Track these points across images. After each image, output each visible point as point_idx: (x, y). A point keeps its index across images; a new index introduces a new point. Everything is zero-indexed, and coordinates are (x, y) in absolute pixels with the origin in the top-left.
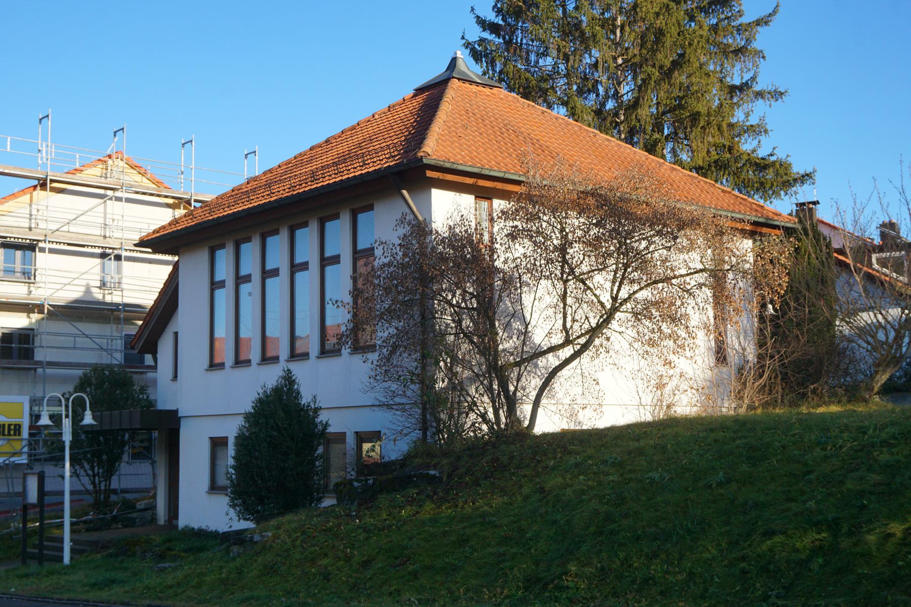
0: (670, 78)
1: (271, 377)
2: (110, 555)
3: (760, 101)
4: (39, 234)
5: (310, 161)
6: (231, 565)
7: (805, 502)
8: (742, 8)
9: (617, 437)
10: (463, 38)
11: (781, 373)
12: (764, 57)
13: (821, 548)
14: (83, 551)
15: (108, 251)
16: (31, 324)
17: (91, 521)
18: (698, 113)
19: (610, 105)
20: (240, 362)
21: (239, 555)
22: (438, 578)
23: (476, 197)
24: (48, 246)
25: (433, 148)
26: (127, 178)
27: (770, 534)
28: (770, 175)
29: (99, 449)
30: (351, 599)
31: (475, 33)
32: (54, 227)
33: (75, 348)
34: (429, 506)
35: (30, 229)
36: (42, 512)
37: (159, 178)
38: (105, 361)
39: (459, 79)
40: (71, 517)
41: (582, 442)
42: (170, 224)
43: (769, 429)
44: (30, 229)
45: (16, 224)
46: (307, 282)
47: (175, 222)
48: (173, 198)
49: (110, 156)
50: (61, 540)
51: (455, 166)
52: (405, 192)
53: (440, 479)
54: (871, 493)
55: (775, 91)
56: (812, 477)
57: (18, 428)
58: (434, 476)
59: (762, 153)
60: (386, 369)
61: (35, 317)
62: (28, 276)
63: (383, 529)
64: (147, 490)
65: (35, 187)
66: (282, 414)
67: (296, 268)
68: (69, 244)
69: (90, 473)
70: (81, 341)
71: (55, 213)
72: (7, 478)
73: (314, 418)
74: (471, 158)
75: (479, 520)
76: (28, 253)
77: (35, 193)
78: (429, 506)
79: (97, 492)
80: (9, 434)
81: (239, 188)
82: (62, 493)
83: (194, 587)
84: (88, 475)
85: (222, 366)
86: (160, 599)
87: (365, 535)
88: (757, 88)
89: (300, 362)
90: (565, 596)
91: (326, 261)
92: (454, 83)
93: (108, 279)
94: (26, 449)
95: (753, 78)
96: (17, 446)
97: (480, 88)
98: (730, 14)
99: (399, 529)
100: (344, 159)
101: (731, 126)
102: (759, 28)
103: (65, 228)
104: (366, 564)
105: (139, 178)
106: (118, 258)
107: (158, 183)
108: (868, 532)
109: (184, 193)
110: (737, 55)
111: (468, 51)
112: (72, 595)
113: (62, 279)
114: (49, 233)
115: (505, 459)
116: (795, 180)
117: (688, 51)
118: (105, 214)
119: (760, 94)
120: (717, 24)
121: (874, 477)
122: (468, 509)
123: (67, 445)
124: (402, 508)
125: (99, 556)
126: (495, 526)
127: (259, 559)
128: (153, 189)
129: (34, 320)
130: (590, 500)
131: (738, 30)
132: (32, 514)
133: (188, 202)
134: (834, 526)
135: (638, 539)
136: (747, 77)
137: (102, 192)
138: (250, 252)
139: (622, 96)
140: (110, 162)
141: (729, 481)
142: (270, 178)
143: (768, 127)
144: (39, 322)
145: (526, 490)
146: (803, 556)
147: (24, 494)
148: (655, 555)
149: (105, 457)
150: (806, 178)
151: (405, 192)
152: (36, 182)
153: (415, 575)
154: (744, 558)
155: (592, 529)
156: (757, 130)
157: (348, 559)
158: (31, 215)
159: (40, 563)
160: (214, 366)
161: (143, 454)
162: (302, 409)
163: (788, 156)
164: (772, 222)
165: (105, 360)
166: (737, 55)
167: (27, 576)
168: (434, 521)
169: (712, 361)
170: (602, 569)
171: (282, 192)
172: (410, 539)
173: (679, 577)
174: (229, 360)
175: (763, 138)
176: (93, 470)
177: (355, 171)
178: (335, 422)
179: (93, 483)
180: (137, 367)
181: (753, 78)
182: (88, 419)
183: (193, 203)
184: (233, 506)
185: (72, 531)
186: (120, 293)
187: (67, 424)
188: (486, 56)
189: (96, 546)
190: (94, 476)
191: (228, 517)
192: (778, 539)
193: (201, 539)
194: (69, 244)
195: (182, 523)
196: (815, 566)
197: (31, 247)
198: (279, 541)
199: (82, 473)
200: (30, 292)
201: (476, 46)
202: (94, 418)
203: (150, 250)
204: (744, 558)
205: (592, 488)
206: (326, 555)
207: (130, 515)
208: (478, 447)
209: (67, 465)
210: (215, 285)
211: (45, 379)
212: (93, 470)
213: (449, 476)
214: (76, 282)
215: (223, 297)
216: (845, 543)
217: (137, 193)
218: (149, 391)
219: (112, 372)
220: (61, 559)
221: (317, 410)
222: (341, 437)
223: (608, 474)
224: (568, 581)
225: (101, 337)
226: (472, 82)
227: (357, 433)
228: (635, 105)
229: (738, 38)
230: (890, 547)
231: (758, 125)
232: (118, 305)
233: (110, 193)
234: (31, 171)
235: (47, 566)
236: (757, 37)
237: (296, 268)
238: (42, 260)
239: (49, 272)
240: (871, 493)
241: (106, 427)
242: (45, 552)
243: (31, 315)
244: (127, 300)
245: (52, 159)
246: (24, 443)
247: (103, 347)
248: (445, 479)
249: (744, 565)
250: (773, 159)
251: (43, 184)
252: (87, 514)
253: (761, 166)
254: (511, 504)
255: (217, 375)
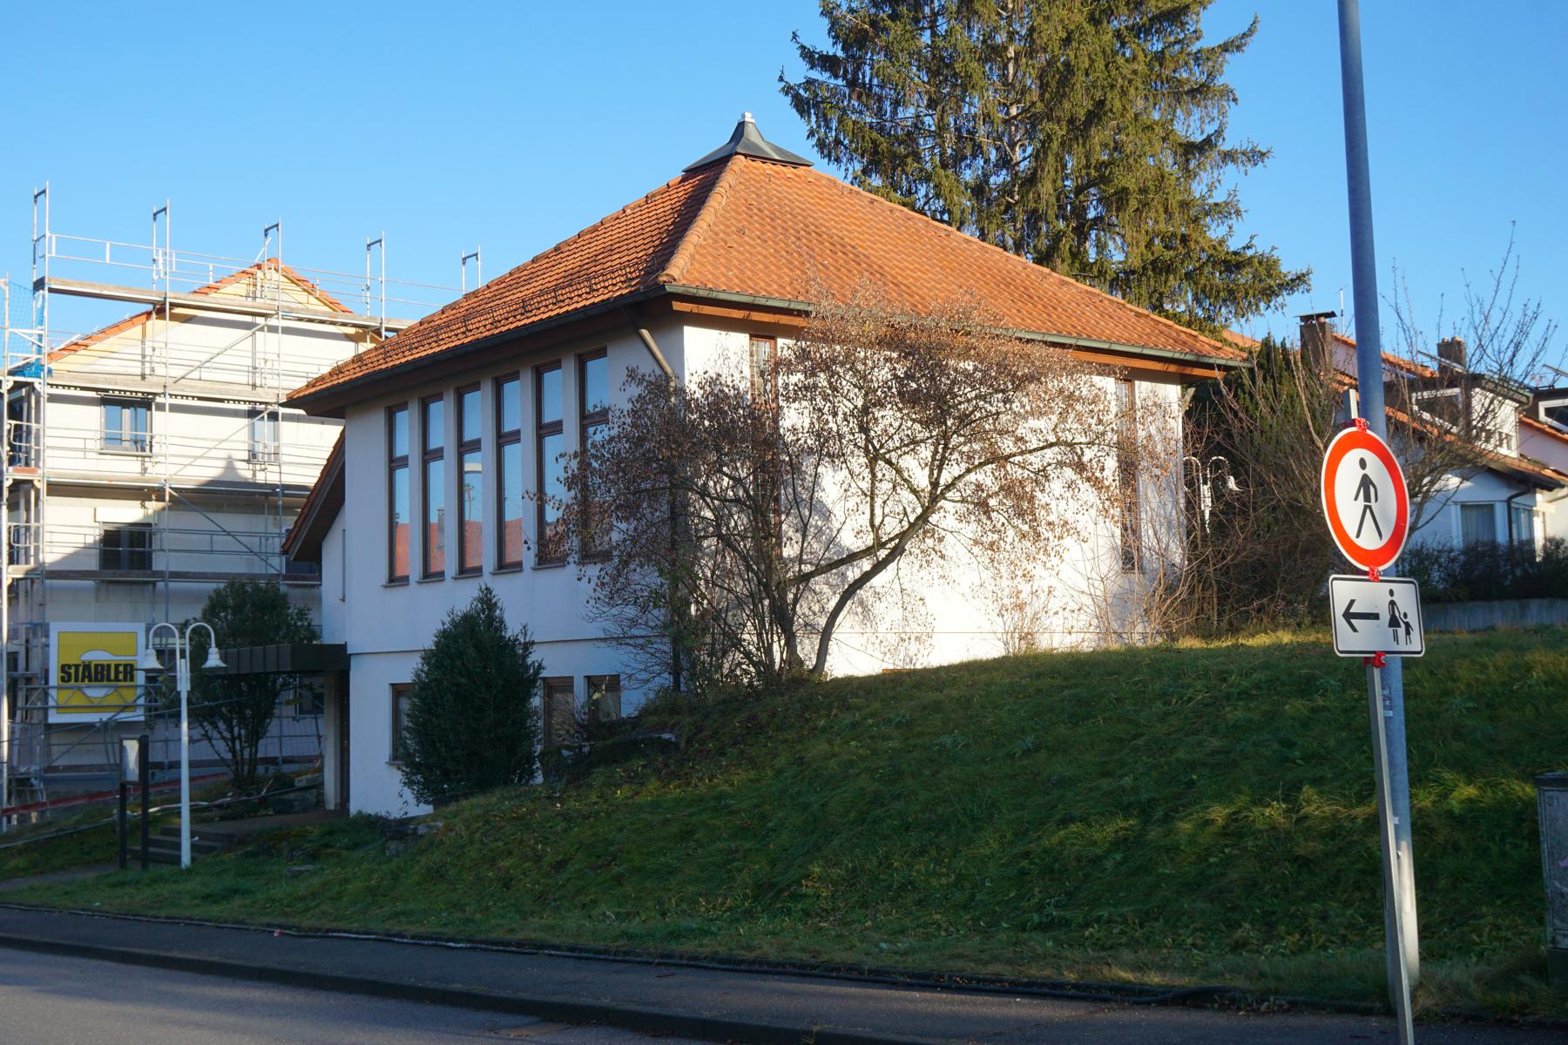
0: (1086, 138)
1: (460, 598)
2: (247, 855)
3: (1231, 167)
4: (156, 385)
5: (527, 282)
6: (384, 867)
7: (1121, 777)
8: (1200, 26)
9: (917, 686)
10: (781, 79)
11: (1218, 582)
12: (1235, 100)
13: (1126, 839)
14: (213, 849)
15: (259, 407)
16: (146, 516)
17: (228, 806)
18: (1125, 190)
19: (997, 180)
20: (430, 575)
21: (398, 854)
22: (648, 884)
23: (752, 336)
24: (168, 401)
25: (681, 271)
26: (284, 297)
27: (1065, 821)
28: (1244, 277)
29: (234, 700)
30: (532, 913)
31: (799, 72)
32: (178, 372)
33: (212, 552)
34: (653, 784)
35: (143, 377)
36: (145, 795)
37: (333, 297)
38: (256, 571)
39: (746, 156)
40: (191, 800)
41: (869, 692)
42: (331, 374)
43: (1109, 674)
44: (143, 377)
45: (122, 370)
46: (518, 458)
47: (358, 359)
48: (354, 326)
49: (259, 267)
50: (178, 833)
51: (714, 295)
52: (645, 332)
53: (676, 745)
54: (1203, 764)
55: (1253, 151)
56: (1141, 742)
57: (129, 671)
58: (668, 741)
59: (1234, 244)
60: (615, 590)
61: (153, 506)
62: (141, 446)
63: (588, 817)
64: (310, 759)
65: (149, 314)
66: (472, 652)
67: (503, 439)
68: (200, 399)
69: (227, 735)
70: (221, 542)
71: (179, 352)
72: (106, 743)
73: (525, 657)
74: (742, 281)
75: (712, 803)
76: (141, 411)
77: (149, 323)
78: (653, 784)
79: (237, 761)
80: (117, 679)
81: (430, 320)
82: (176, 765)
83: (332, 899)
84: (223, 738)
85: (404, 580)
86: (286, 915)
87: (564, 825)
88: (1225, 146)
89: (511, 576)
90: (800, 906)
91: (545, 430)
92: (739, 162)
93: (259, 448)
94: (141, 701)
95: (1219, 133)
96: (129, 696)
97: (779, 168)
98: (1182, 36)
99: (609, 815)
100: (571, 280)
101: (1184, 205)
102: (1227, 56)
103: (195, 375)
104: (560, 866)
105: (303, 297)
106: (273, 416)
107: (332, 304)
108: (1181, 819)
109: (371, 319)
110: (1194, 97)
111: (789, 99)
112: (174, 912)
113: (191, 451)
114: (170, 382)
115: (764, 717)
116: (1281, 286)
117: (1109, 96)
118: (254, 353)
119: (1229, 156)
120: (1162, 52)
121: (1215, 743)
122: (702, 789)
123: (184, 696)
124: (619, 786)
125: (232, 855)
126: (732, 812)
127: (424, 859)
128: (324, 314)
129: (150, 512)
130: (858, 775)
131: (1197, 59)
132: (133, 798)
133: (378, 332)
134: (1145, 811)
135: (907, 829)
136: (1210, 129)
137: (248, 320)
138: (478, 405)
139: (1018, 164)
140: (260, 274)
141: (1037, 748)
142: (474, 304)
143: (1242, 207)
144: (158, 513)
145: (781, 761)
146: (1099, 851)
147: (121, 765)
148: (923, 851)
149: (248, 712)
150: (1300, 279)
151: (645, 332)
152: (150, 307)
153: (619, 880)
154: (1027, 855)
155: (852, 815)
156: (1225, 211)
157: (538, 858)
158: (144, 356)
159: (145, 867)
160: (395, 580)
161: (313, 707)
162: (506, 645)
163: (1273, 248)
164: (1206, 360)
165: (258, 568)
166: (1194, 97)
167: (122, 884)
168: (655, 805)
169: (1118, 566)
170: (854, 870)
171: (481, 329)
172: (620, 830)
173: (944, 881)
174: (415, 572)
175: (1233, 221)
176: (232, 732)
177: (580, 300)
178: (552, 662)
179: (233, 751)
180: (304, 579)
181: (1219, 133)
182: (214, 660)
183: (384, 333)
184: (409, 783)
185: (193, 821)
186: (276, 469)
187: (183, 668)
188: (816, 105)
189: (230, 841)
190: (233, 740)
191: (401, 801)
192: (1073, 827)
193: (377, 827)
194: (200, 399)
195: (354, 807)
196: (1109, 864)
197: (144, 403)
198: (452, 834)
199: (216, 735)
200: (145, 470)
201: (802, 92)
202: (224, 658)
203: (302, 412)
204: (1027, 855)
205: (862, 758)
206: (510, 853)
207: (286, 797)
208: (737, 699)
209: (185, 725)
210: (395, 463)
211: (168, 597)
212: (232, 732)
213: (689, 741)
214: (213, 453)
215: (406, 479)
216: (1154, 834)
217: (300, 319)
218: (312, 615)
219: (257, 588)
220: (178, 859)
221: (528, 646)
222: (566, 684)
223: (890, 738)
224: (807, 888)
225: (250, 534)
226: (765, 159)
227: (588, 678)
228: (1031, 180)
229: (1196, 70)
230: (1205, 838)
231: (1227, 204)
232: (274, 487)
233: (260, 320)
234: (141, 292)
235: (155, 870)
236: (1226, 68)
237: (503, 439)
238: (162, 422)
239: (170, 440)
240: (1203, 764)
241: (245, 670)
242: (151, 849)
243: (147, 504)
244: (288, 479)
245: (172, 273)
246: (140, 691)
247: (253, 548)
248: (683, 745)
249: (1024, 863)
250: (1249, 253)
251: (160, 310)
252: (224, 795)
253: (1233, 264)
254: (758, 781)
255: (400, 593)
